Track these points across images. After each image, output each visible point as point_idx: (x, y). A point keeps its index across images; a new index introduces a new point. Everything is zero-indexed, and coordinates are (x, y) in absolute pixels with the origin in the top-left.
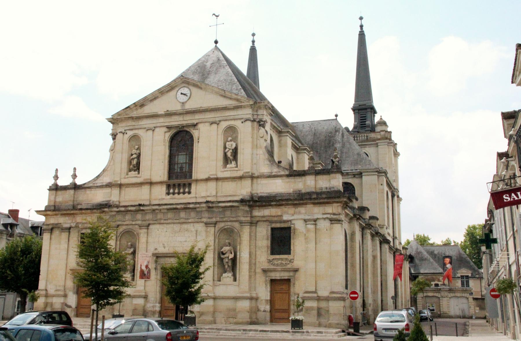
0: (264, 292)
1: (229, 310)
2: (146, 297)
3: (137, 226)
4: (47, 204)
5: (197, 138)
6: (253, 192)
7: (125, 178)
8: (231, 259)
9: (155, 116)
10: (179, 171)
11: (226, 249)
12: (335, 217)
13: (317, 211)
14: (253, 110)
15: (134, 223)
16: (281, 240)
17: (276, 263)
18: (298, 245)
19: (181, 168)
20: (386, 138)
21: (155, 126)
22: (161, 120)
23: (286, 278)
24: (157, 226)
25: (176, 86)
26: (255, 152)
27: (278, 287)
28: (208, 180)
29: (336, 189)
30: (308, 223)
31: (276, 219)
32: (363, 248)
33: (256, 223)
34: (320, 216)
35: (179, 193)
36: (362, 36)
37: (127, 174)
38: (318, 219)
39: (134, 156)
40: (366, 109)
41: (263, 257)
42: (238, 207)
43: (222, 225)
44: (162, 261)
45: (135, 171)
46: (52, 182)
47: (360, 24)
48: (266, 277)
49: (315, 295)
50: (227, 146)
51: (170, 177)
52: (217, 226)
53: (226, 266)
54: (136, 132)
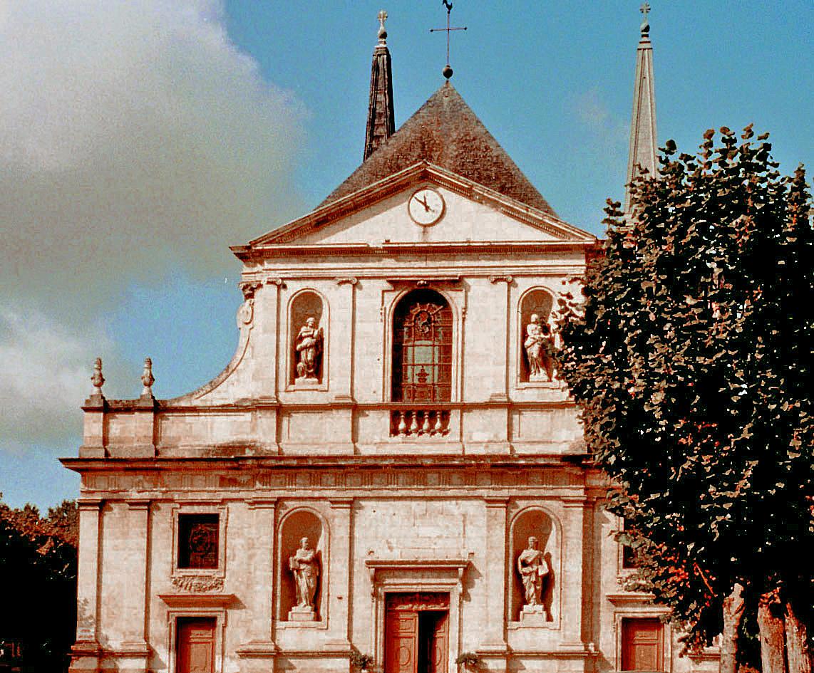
10: (416, 382)
19: (423, 375)
21: (359, 275)
37: (293, 382)
39: (306, 342)
42: (561, 467)
45: (309, 375)
50: (529, 332)
51: (397, 394)
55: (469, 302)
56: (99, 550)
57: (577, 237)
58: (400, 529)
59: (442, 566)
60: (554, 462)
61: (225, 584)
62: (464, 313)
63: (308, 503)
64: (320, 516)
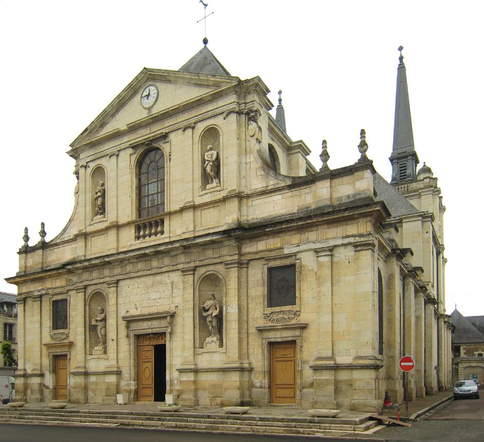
0: (258, 358)
1: (214, 386)
2: (118, 373)
3: (105, 285)
4: (18, 271)
5: (168, 153)
6: (243, 219)
7: (90, 225)
8: (216, 316)
9: (117, 135)
11: (209, 303)
12: (362, 239)
13: (333, 235)
14: (239, 97)
15: (102, 281)
16: (282, 285)
17: (275, 318)
18: (307, 290)
20: (431, 186)
22: (126, 139)
23: (290, 339)
24: (127, 282)
25: (140, 87)
26: (243, 161)
27: (280, 353)
28: (182, 210)
29: (363, 196)
30: (320, 254)
31: (273, 254)
32: (404, 302)
33: (248, 264)
34: (339, 242)
35: (150, 235)
36: (402, 68)
37: (92, 220)
38: (336, 246)
39: (99, 194)
40: (406, 157)
41: (258, 312)
42: (221, 242)
43: (202, 271)
44: (134, 326)
46: (22, 243)
47: (399, 56)
48: (263, 339)
49: (332, 363)
52: (196, 274)
53: (211, 328)
54: (99, 162)
55: (172, 148)
56: (41, 319)
57: (227, 82)
58: (138, 296)
59: (153, 316)
60: (215, 238)
61: (70, 337)
62: (170, 155)
63: (211, 268)
64: (104, 294)
